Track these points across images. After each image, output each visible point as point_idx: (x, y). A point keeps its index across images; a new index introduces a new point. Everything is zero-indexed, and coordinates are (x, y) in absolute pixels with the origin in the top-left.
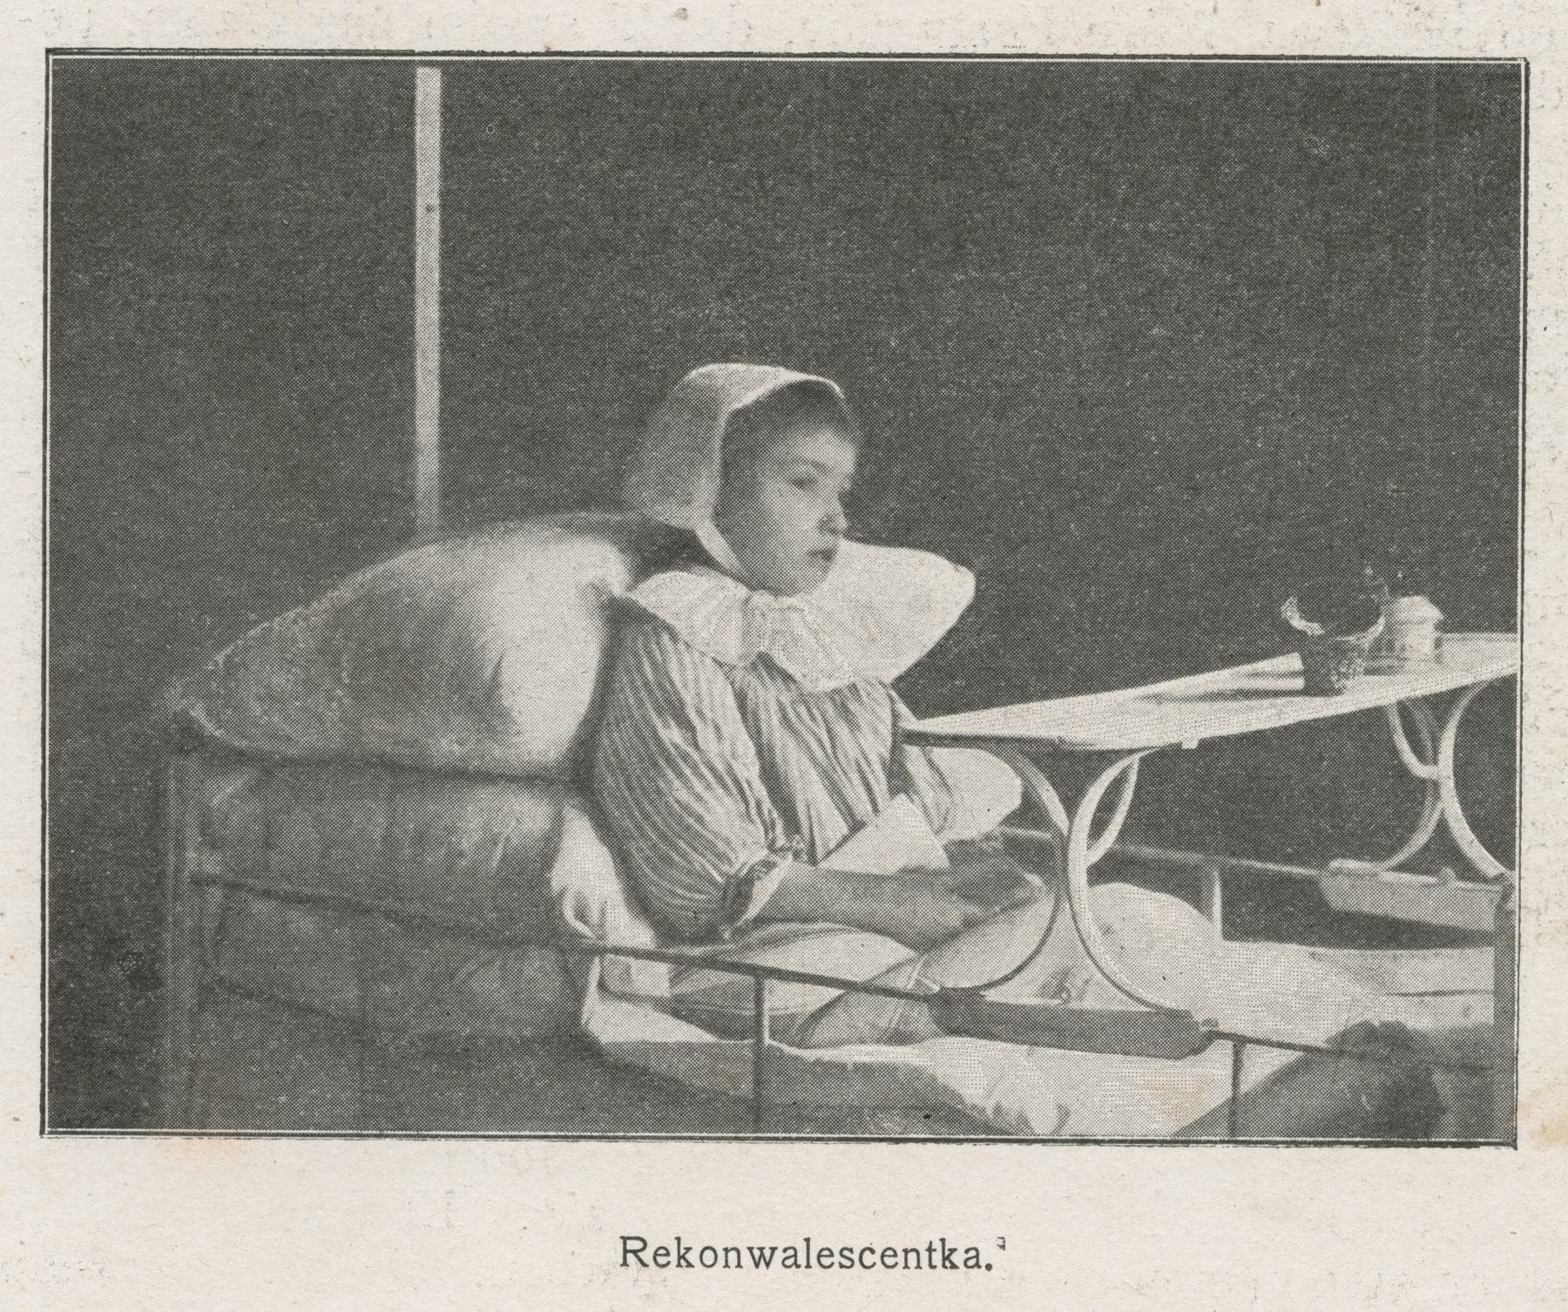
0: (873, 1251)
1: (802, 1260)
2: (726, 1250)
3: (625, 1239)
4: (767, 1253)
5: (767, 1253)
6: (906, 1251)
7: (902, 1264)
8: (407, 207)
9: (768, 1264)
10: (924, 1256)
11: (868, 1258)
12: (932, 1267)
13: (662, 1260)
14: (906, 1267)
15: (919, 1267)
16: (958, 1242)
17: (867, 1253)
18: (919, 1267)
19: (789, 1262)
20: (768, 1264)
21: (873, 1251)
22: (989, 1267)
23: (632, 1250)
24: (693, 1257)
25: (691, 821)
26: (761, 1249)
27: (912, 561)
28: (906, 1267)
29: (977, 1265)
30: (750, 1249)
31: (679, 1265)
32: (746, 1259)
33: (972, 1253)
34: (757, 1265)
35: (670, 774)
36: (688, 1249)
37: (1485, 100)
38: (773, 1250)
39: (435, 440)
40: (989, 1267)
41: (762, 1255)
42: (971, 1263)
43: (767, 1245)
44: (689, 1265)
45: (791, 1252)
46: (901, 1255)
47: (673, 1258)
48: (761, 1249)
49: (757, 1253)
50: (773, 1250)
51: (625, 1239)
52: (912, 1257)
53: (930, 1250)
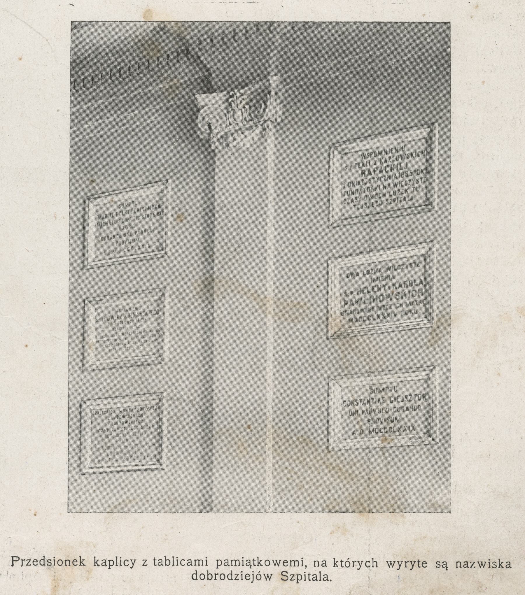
0: (369, 562)
1: (318, 578)
3: (13, 557)
4: (393, 563)
7: (372, 566)
9: (484, 567)
10: (303, 577)
12: (310, 580)
14: (291, 566)
15: (199, 565)
16: (263, 558)
17: (126, 561)
18: (199, 565)
21: (369, 562)
22: (331, 580)
24: (262, 563)
28: (291, 566)
30: (273, 561)
31: (80, 565)
32: (476, 564)
34: (480, 567)
36: (261, 561)
38: (280, 561)
39: (268, 228)
41: (482, 564)
45: (160, 561)
46: (289, 562)
47: (78, 563)
48: (482, 562)
49: (389, 563)
50: (362, 562)
51: (13, 557)
53: (254, 560)
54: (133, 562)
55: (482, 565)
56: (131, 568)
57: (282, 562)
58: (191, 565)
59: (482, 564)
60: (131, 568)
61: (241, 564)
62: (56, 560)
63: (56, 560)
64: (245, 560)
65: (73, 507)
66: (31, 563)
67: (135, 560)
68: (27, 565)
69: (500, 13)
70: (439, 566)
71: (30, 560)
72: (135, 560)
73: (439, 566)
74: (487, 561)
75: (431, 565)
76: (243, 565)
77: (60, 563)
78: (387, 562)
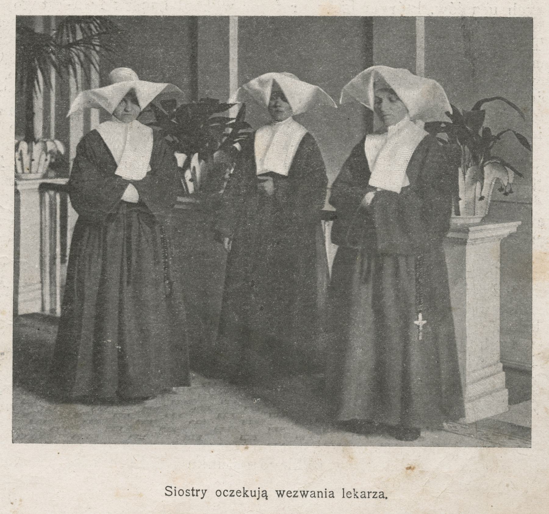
0: (227, 491)
2: (318, 492)
5: (282, 492)
6: (318, 492)
8: (154, 19)
9: (306, 496)
11: (226, 493)
13: (239, 494)
15: (322, 497)
16: (359, 489)
17: (226, 492)
18: (322, 497)
19: (313, 495)
20: (306, 496)
21: (227, 491)
23: (382, 496)
25: (125, 247)
26: (280, 491)
27: (106, 415)
29: (383, 497)
31: (244, 496)
33: (264, 492)
34: (303, 496)
35: (71, 71)
36: (247, 491)
37: (521, 30)
38: (308, 492)
40: (386, 498)
41: (304, 493)
42: (363, 496)
43: (282, 490)
44: (247, 496)
48: (304, 491)
49: (279, 492)
52: (320, 494)
54: (205, 492)
55: (304, 494)
56: (202, 498)
57: (285, 493)
58: (315, 496)
59: (304, 493)
60: (202, 498)
61: (324, 496)
62: (177, 490)
63: (177, 490)
64: (328, 491)
65: (20, 436)
66: (234, 493)
67: (206, 490)
68: (373, 497)
69: (389, 196)
70: (169, 493)
71: (233, 491)
72: (206, 490)
73: (169, 493)
74: (257, 490)
75: (338, 494)
76: (326, 497)
77: (181, 493)
78: (277, 491)
